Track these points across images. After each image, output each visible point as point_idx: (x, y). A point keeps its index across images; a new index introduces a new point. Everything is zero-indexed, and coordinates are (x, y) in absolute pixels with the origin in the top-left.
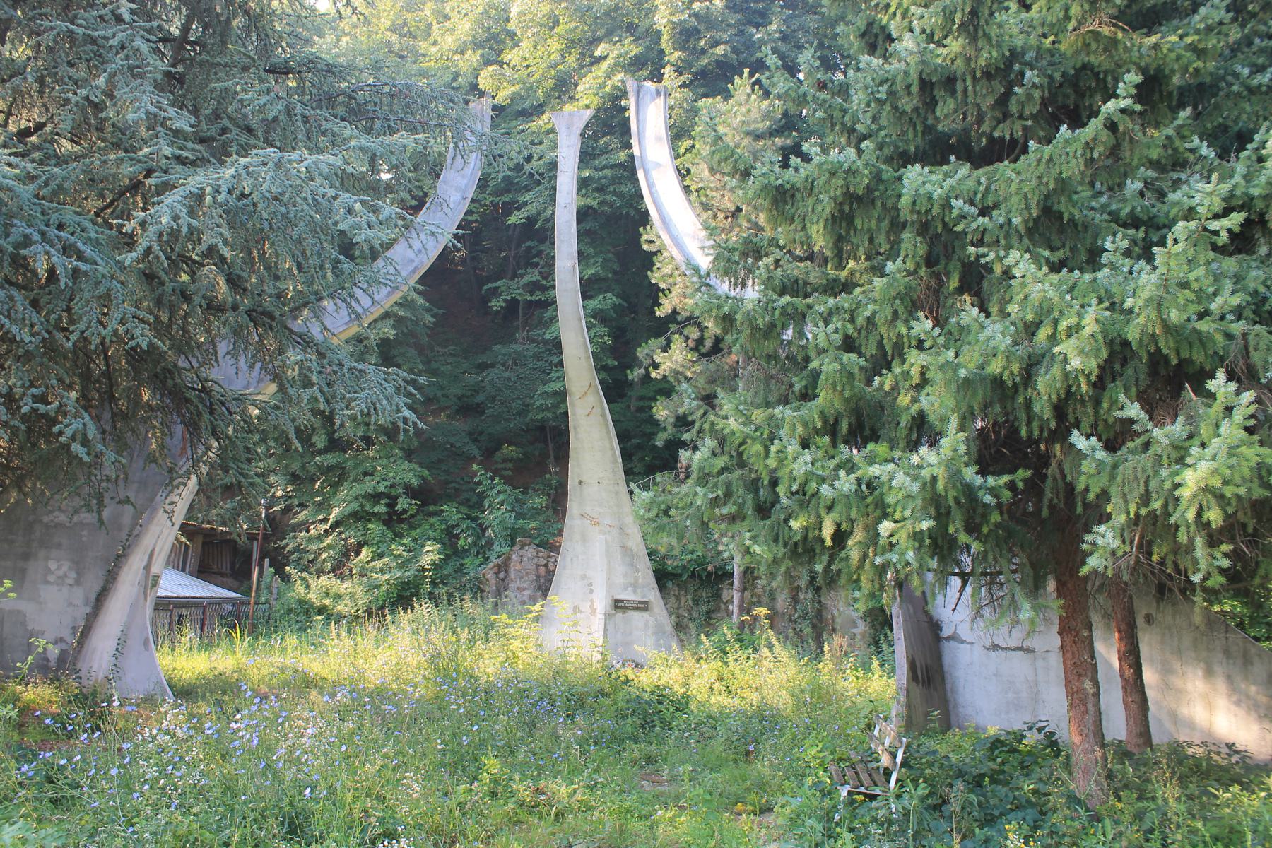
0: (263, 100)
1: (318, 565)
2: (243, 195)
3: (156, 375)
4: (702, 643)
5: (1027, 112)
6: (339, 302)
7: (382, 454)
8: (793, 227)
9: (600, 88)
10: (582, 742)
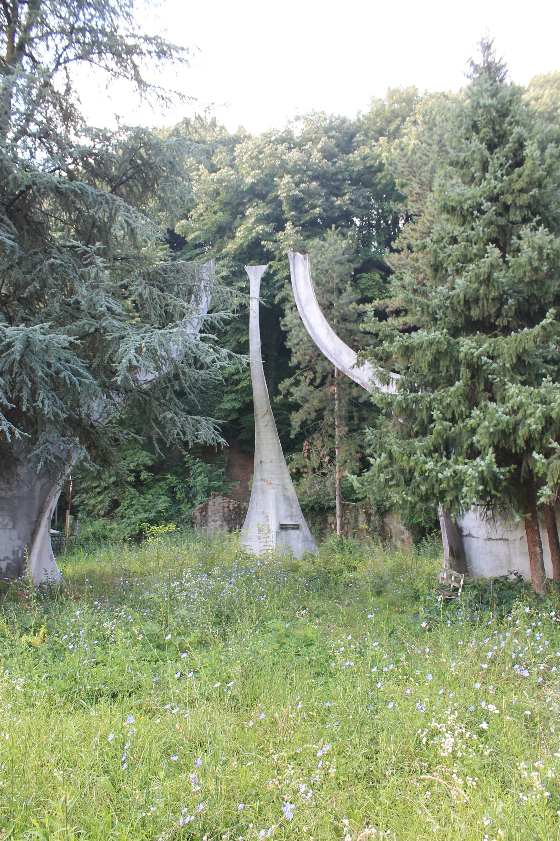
5: (509, 315)
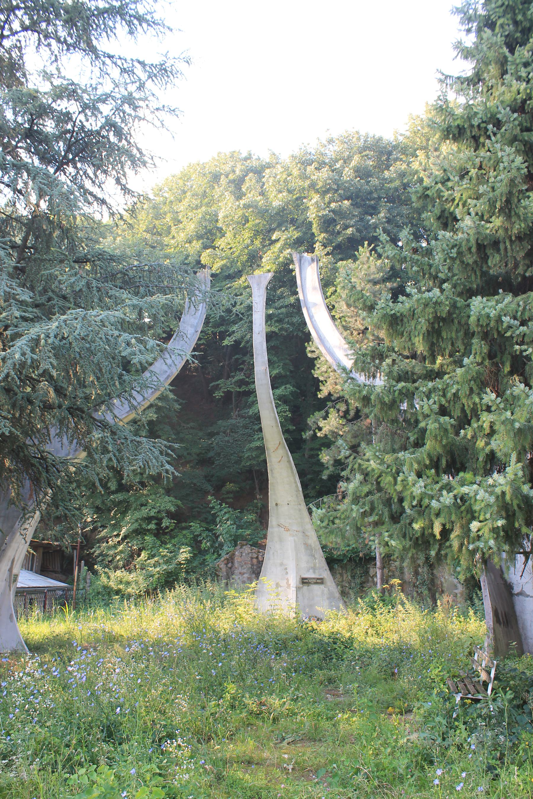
0: (73, 279)
1: (115, 564)
2: (63, 338)
3: (13, 450)
4: (358, 603)
6: (123, 399)
7: (151, 492)
8: (403, 339)
9: (276, 259)
10: (287, 671)
